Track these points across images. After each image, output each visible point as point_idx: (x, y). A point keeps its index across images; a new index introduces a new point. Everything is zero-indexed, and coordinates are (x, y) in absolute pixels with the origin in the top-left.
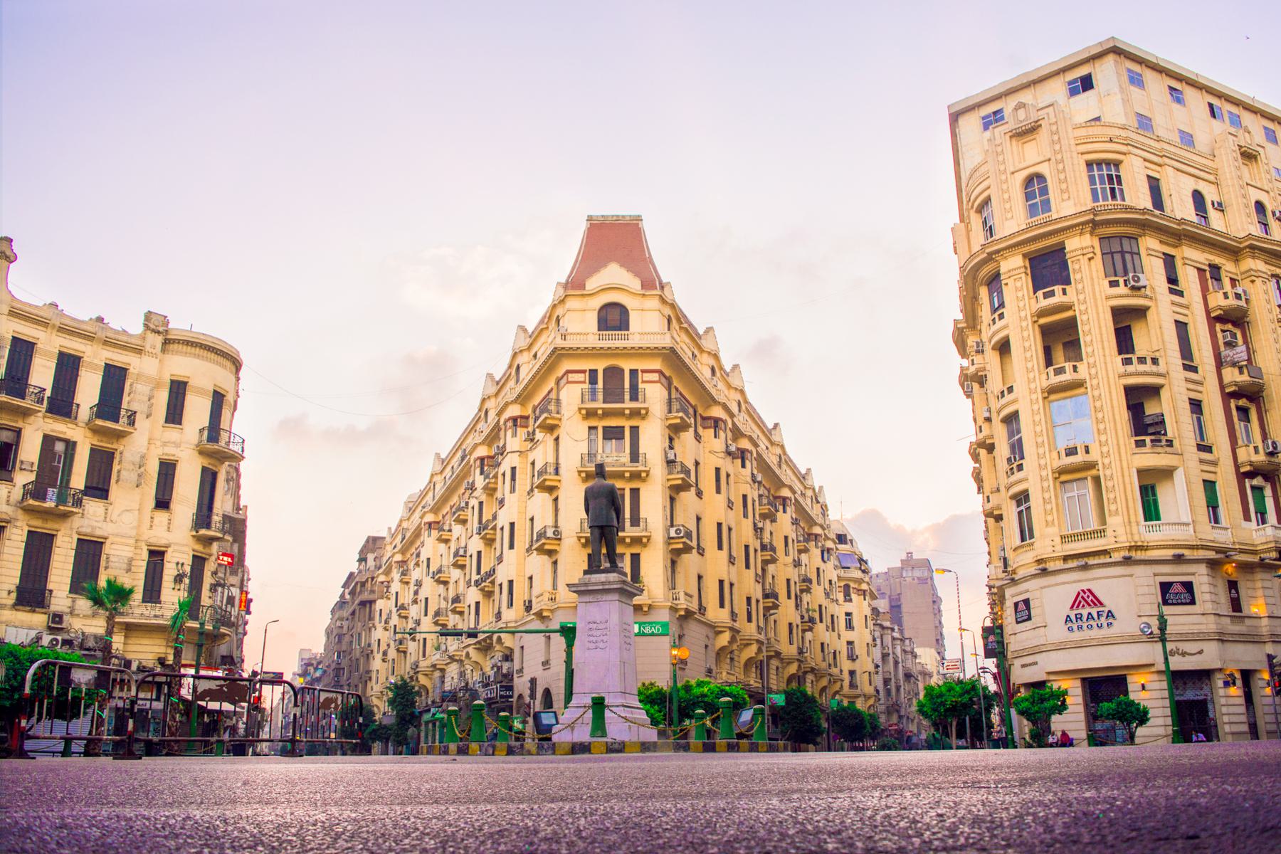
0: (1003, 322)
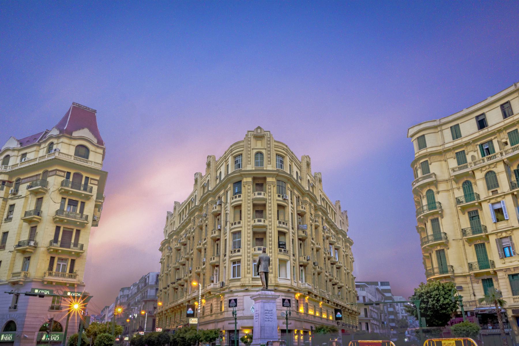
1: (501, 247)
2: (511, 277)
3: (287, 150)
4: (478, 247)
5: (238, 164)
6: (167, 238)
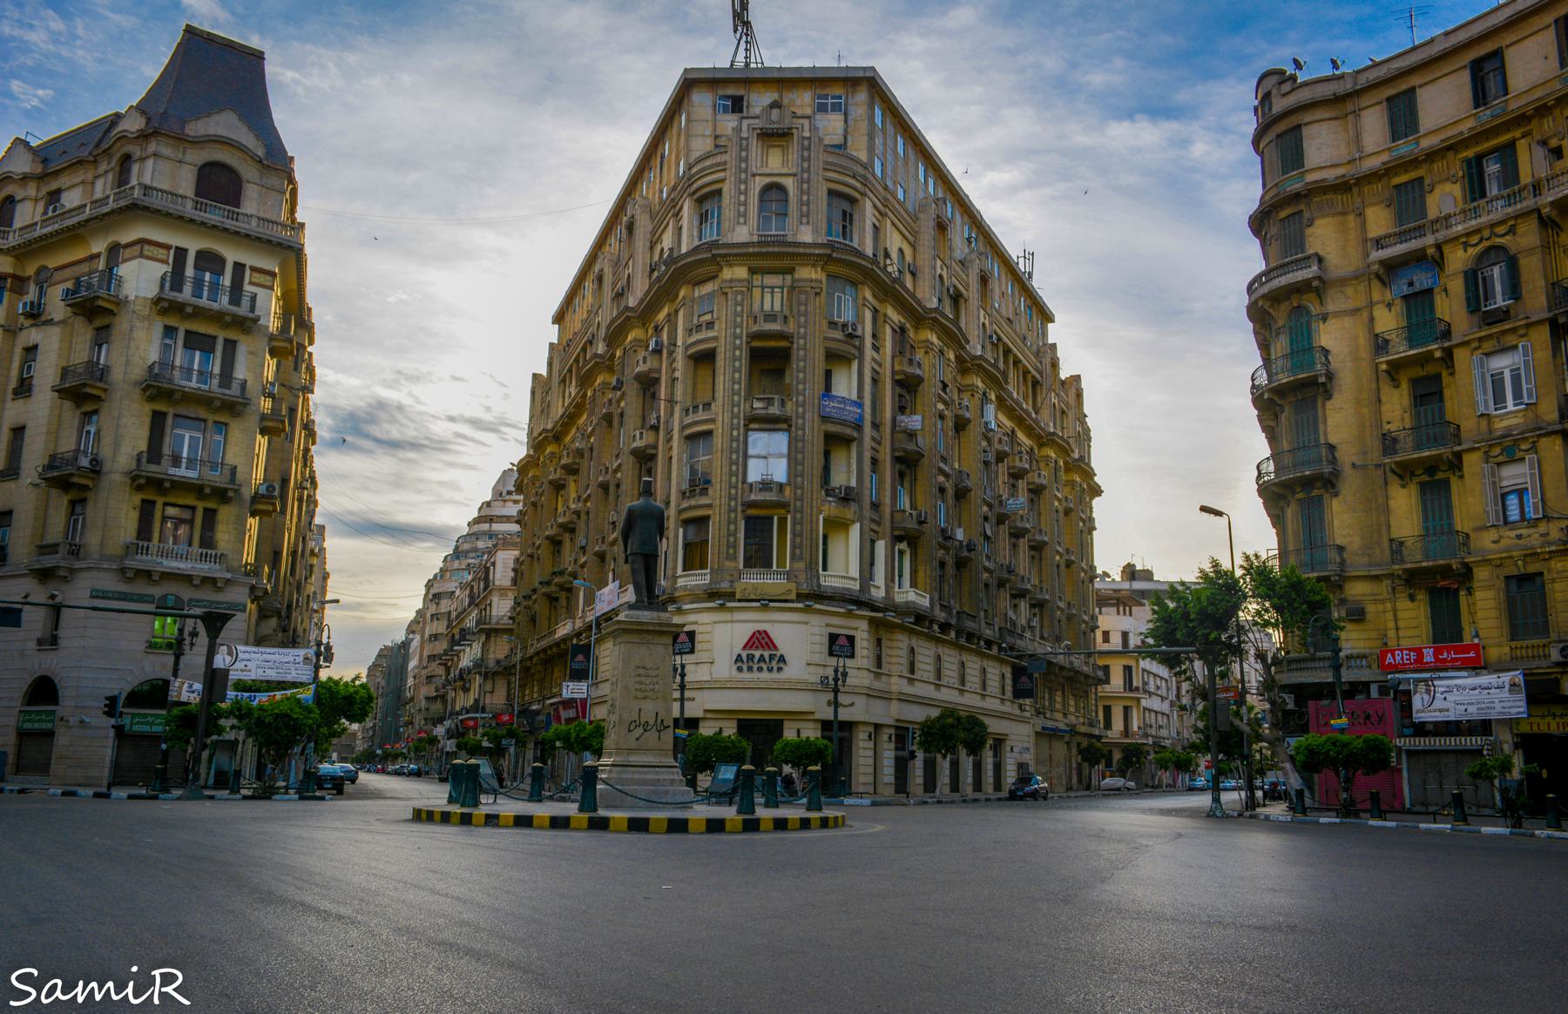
0: (711, 334)
1: (1495, 491)
2: (1513, 586)
3: (866, 179)
6: (532, 452)
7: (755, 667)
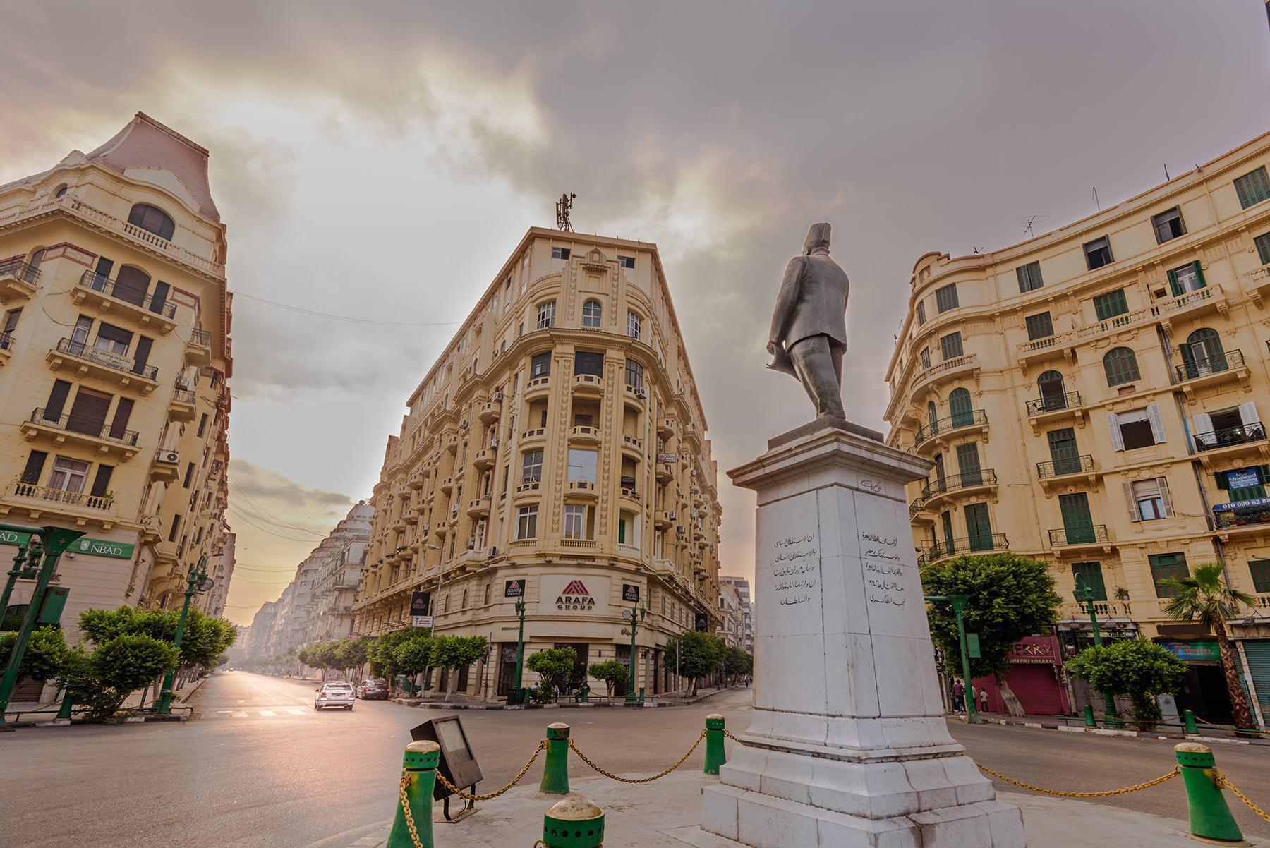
2: (1155, 560)
4: (1067, 501)
5: (545, 319)
7: (571, 606)
